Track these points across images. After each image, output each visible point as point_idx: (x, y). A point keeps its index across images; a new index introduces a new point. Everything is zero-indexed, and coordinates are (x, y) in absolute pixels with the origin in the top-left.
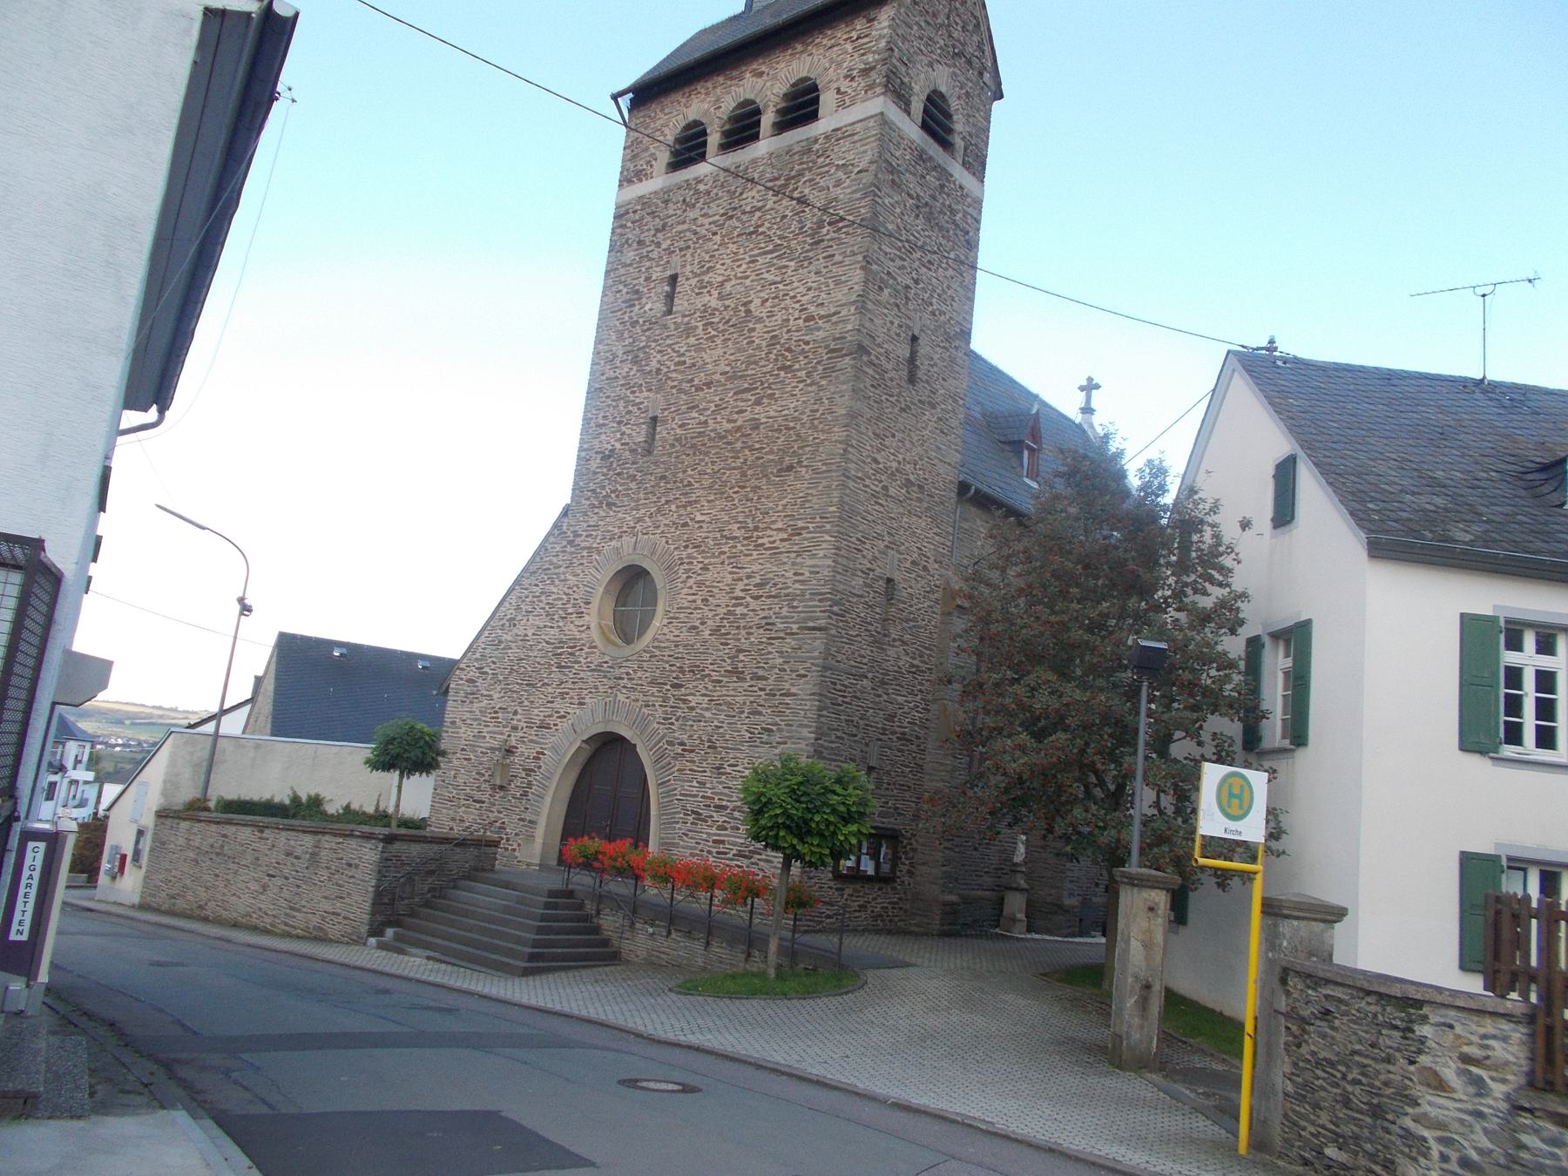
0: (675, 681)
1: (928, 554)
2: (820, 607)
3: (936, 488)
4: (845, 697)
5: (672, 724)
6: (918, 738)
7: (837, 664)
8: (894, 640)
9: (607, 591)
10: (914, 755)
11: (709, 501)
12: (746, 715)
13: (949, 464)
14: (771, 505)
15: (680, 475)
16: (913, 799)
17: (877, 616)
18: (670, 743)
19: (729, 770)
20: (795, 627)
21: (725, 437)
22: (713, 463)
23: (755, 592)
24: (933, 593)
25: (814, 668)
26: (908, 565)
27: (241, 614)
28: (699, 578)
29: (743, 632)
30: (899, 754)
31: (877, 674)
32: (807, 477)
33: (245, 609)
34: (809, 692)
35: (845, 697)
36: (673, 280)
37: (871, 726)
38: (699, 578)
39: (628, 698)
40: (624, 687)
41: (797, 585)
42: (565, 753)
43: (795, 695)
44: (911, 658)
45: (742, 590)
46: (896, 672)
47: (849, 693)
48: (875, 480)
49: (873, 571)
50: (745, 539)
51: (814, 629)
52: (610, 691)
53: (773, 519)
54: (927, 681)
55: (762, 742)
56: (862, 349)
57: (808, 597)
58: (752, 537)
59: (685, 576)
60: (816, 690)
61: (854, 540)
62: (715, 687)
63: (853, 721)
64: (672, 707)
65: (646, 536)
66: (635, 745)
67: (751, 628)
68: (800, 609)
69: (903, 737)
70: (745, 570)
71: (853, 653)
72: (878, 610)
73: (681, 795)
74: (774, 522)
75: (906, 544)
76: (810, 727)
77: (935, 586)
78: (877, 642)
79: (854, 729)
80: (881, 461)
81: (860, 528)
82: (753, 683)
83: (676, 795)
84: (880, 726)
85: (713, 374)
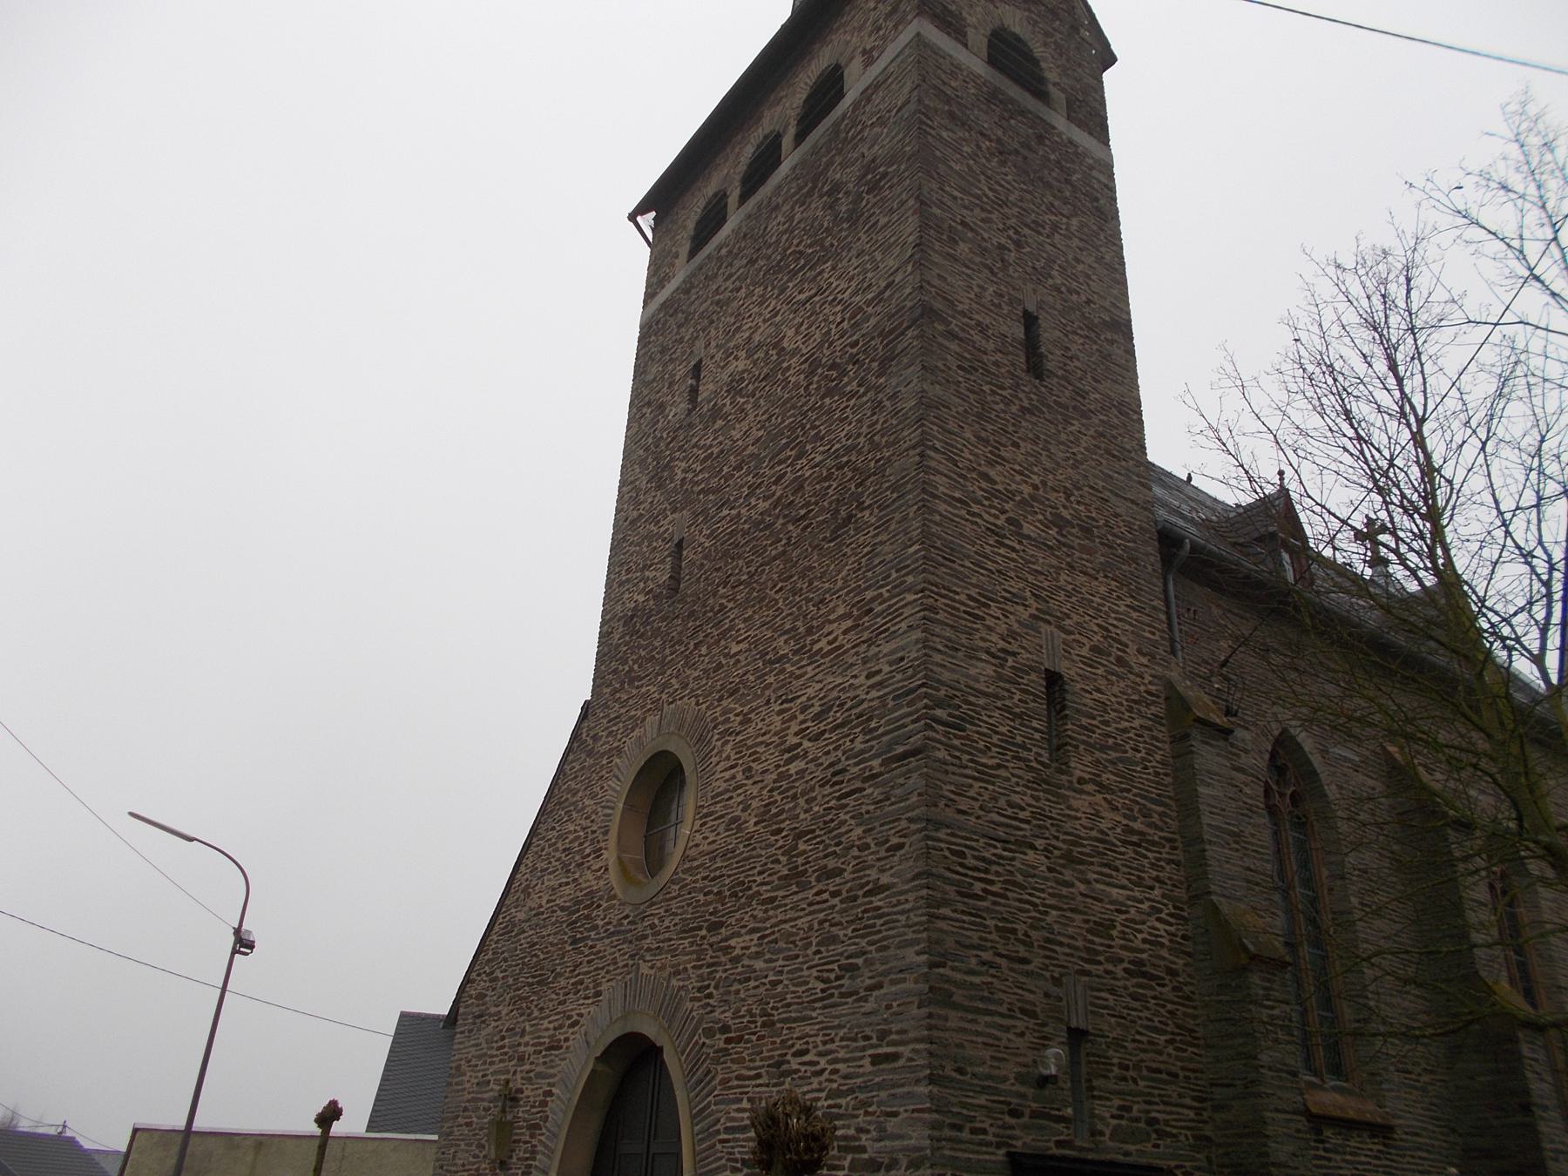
0: (713, 919)
1: (1124, 639)
2: (910, 714)
3: (1114, 535)
4: (992, 882)
5: (710, 996)
6: (1172, 973)
7: (962, 818)
8: (1081, 781)
9: (629, 805)
10: (1170, 1006)
11: (745, 620)
12: (814, 948)
13: (1133, 502)
14: (827, 585)
15: (711, 601)
16: (1188, 1101)
17: (1037, 736)
18: (709, 1033)
19: (794, 1063)
20: (876, 763)
21: (763, 521)
22: (748, 564)
23: (814, 729)
24: (1148, 706)
25: (914, 827)
26: (1085, 652)
27: (234, 952)
28: (739, 738)
29: (801, 801)
30: (1136, 1004)
31: (1054, 842)
32: (873, 520)
33: (243, 944)
34: (909, 876)
35: (992, 882)
36: (697, 369)
37: (1061, 944)
38: (739, 738)
39: (652, 968)
40: (649, 950)
41: (874, 694)
42: (575, 1087)
43: (887, 887)
44: (1125, 816)
45: (796, 734)
46: (1097, 840)
47: (998, 874)
48: (990, 506)
49: (1014, 654)
50: (796, 652)
51: (905, 756)
52: (631, 962)
53: (832, 605)
54: (1169, 862)
55: (842, 995)
56: (928, 313)
57: (891, 704)
58: (804, 646)
59: (719, 743)
60: (921, 866)
61: (963, 597)
62: (766, 911)
63: (1014, 931)
64: (710, 965)
65: (673, 706)
66: (661, 1049)
67: (812, 789)
68: (881, 730)
69: (1138, 970)
70: (799, 701)
71: (995, 799)
72: (1035, 724)
73: (727, 1130)
74: (833, 610)
75: (1075, 618)
76: (917, 942)
77: (1147, 692)
78: (1044, 781)
79: (1021, 948)
80: (998, 479)
81: (974, 581)
82: (821, 886)
83: (718, 1132)
84: (1080, 944)
85: (744, 449)
